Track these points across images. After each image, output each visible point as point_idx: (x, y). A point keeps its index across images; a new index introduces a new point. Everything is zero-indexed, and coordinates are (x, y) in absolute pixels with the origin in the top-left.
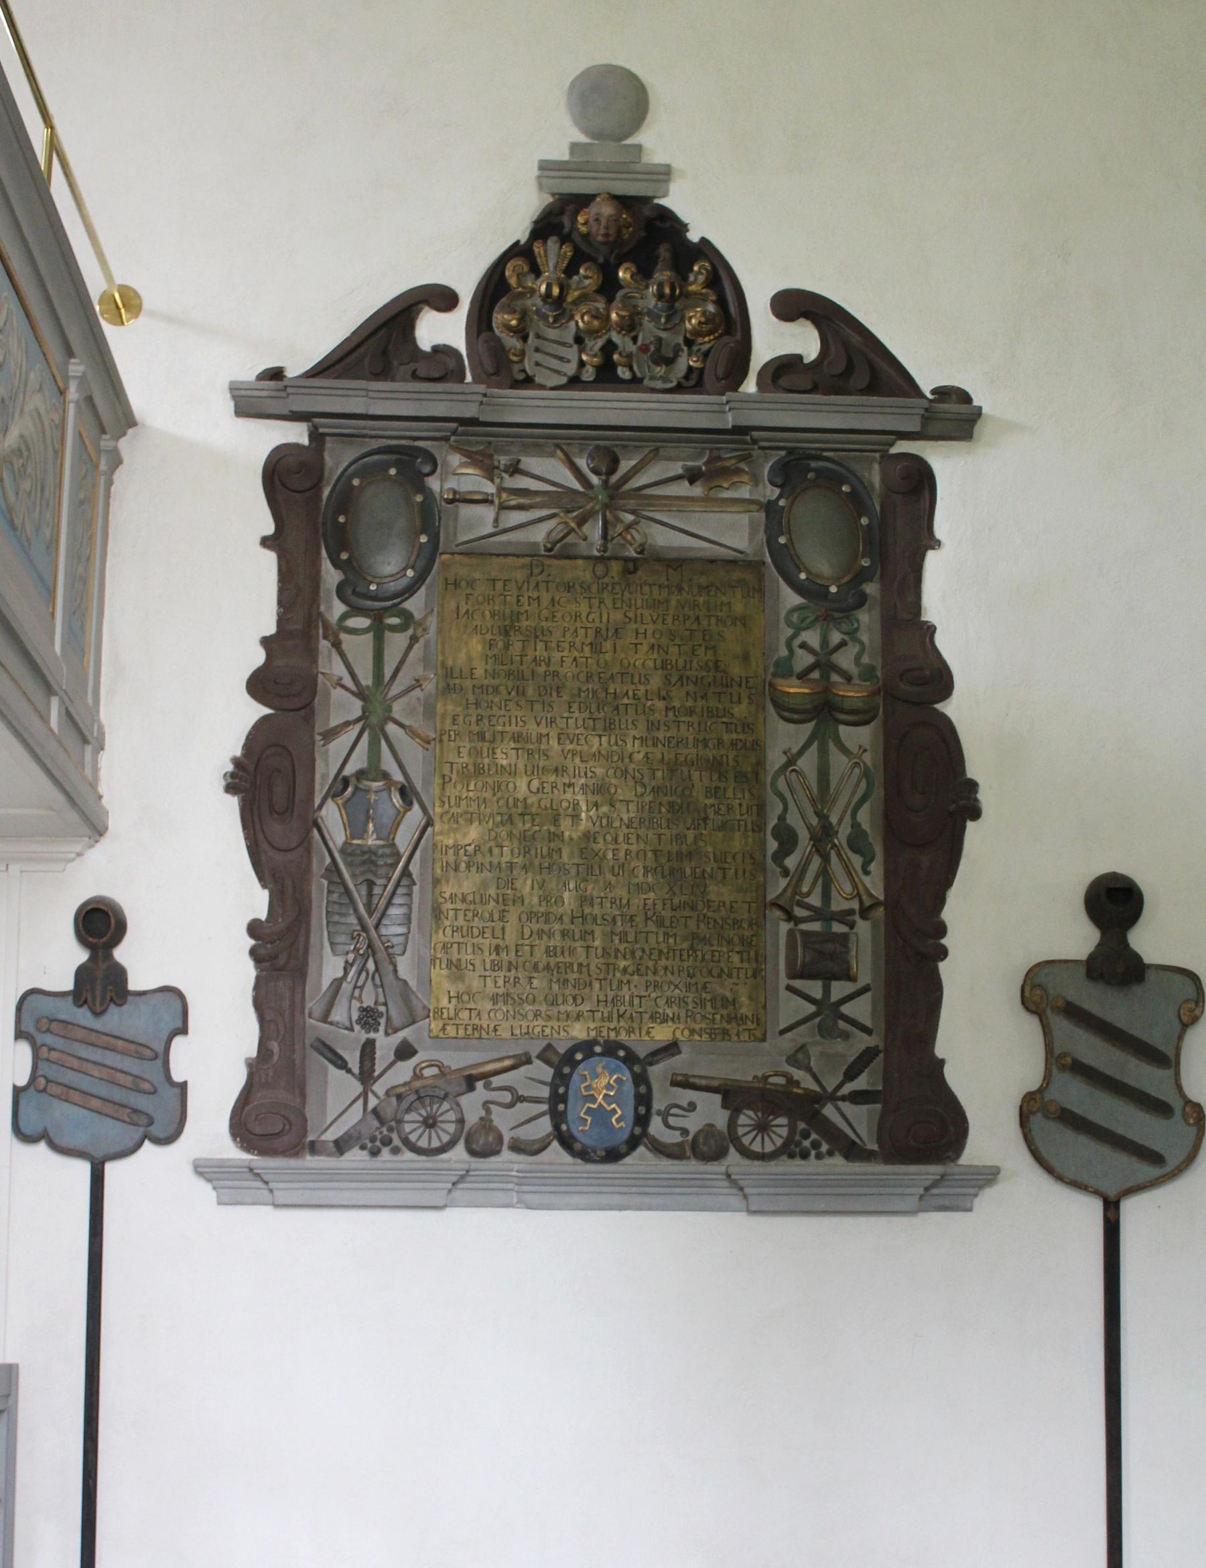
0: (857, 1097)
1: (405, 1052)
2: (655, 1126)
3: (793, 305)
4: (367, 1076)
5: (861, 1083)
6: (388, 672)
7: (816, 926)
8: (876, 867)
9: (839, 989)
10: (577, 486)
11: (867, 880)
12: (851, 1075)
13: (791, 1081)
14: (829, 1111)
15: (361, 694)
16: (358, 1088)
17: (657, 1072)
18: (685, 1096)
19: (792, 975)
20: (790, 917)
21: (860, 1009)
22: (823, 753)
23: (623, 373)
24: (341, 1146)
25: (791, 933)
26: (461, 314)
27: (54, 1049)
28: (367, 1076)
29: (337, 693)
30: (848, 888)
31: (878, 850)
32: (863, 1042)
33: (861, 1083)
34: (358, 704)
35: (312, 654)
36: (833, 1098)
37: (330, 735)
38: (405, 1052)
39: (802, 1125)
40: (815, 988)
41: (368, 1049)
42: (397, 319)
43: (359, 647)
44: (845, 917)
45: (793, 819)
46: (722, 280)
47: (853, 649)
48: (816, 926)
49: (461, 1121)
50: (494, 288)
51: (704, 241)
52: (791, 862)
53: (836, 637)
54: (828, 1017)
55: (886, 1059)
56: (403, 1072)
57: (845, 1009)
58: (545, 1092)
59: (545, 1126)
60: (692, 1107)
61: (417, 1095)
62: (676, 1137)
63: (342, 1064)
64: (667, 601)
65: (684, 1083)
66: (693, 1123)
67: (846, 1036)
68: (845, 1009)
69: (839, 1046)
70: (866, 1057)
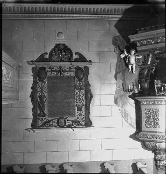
0: (83, 121)
1: (45, 119)
2: (66, 124)
3: (76, 53)
4: (42, 121)
5: (83, 120)
6: (43, 86)
7: (79, 107)
8: (84, 102)
9: (81, 112)
10: (58, 70)
11: (83, 103)
12: (82, 119)
13: (77, 120)
14: (80, 122)
15: (40, 88)
16: (41, 122)
17: (66, 119)
18: (69, 121)
19: (77, 111)
20: (77, 106)
21: (83, 114)
22: (80, 92)
23: (99, 52)
24: (40, 127)
25: (77, 108)
26: (48, 55)
27: (148, 39)
28: (42, 121)
29: (39, 88)
30: (82, 104)
31: (84, 101)
32: (83, 116)
33: (83, 120)
34: (40, 89)
35: (36, 85)
36: (80, 121)
37: (38, 92)
38: (45, 119)
39: (78, 124)
40: (79, 112)
41: (42, 119)
42: (43, 55)
43: (40, 84)
44: (82, 106)
45: (77, 98)
46: (71, 52)
47: (82, 83)
48: (79, 107)
49: (50, 124)
50: (51, 52)
51: (69, 48)
52: (77, 102)
53: (81, 82)
54: (80, 115)
55: (85, 118)
56: (45, 120)
57: (82, 114)
58: (57, 121)
59: (57, 125)
60: (69, 122)
61: (45, 123)
62: (68, 125)
63: (40, 120)
64: (18, 103)
65: (69, 120)
66: (69, 124)
67: (82, 116)
68: (82, 114)
69: (81, 117)
70: (83, 118)
